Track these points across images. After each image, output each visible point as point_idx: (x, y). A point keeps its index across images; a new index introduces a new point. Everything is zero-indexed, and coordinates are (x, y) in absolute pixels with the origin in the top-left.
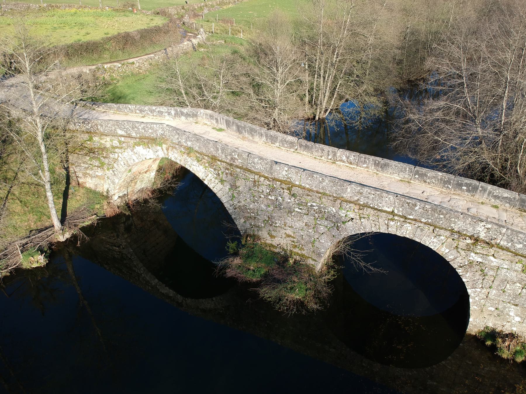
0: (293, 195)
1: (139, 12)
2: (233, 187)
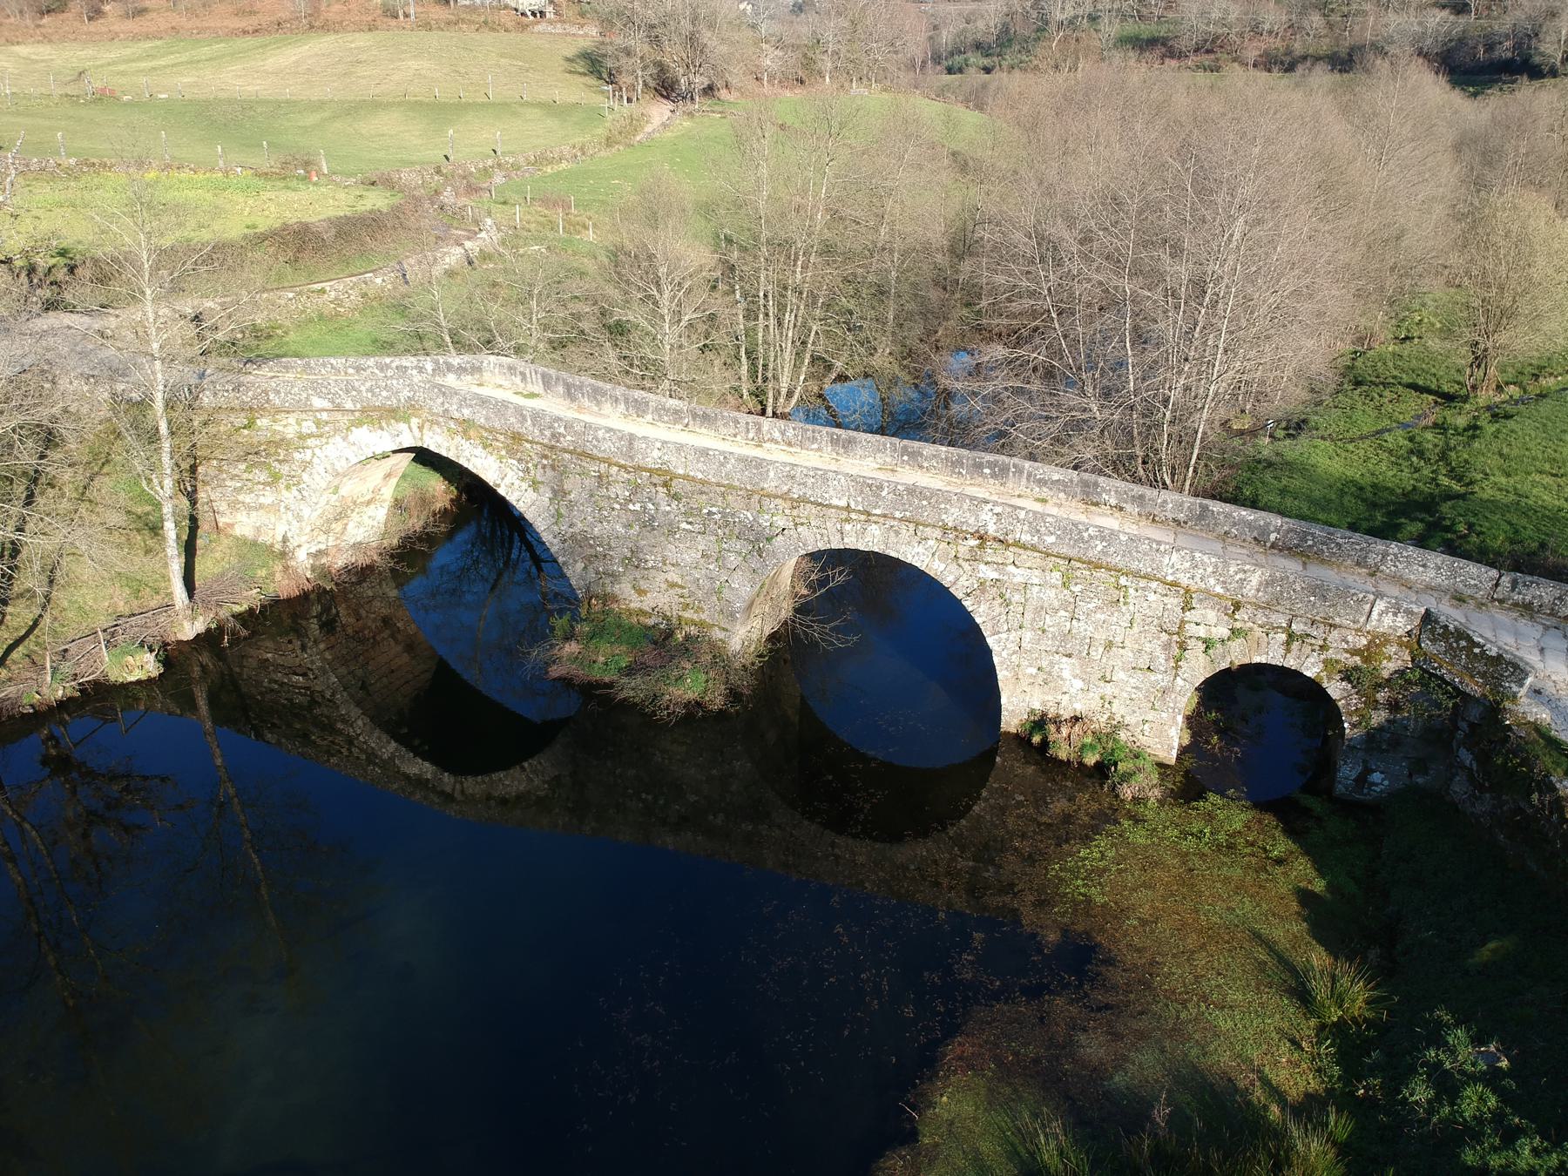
0: (676, 497)
1: (324, 180)
2: (559, 493)
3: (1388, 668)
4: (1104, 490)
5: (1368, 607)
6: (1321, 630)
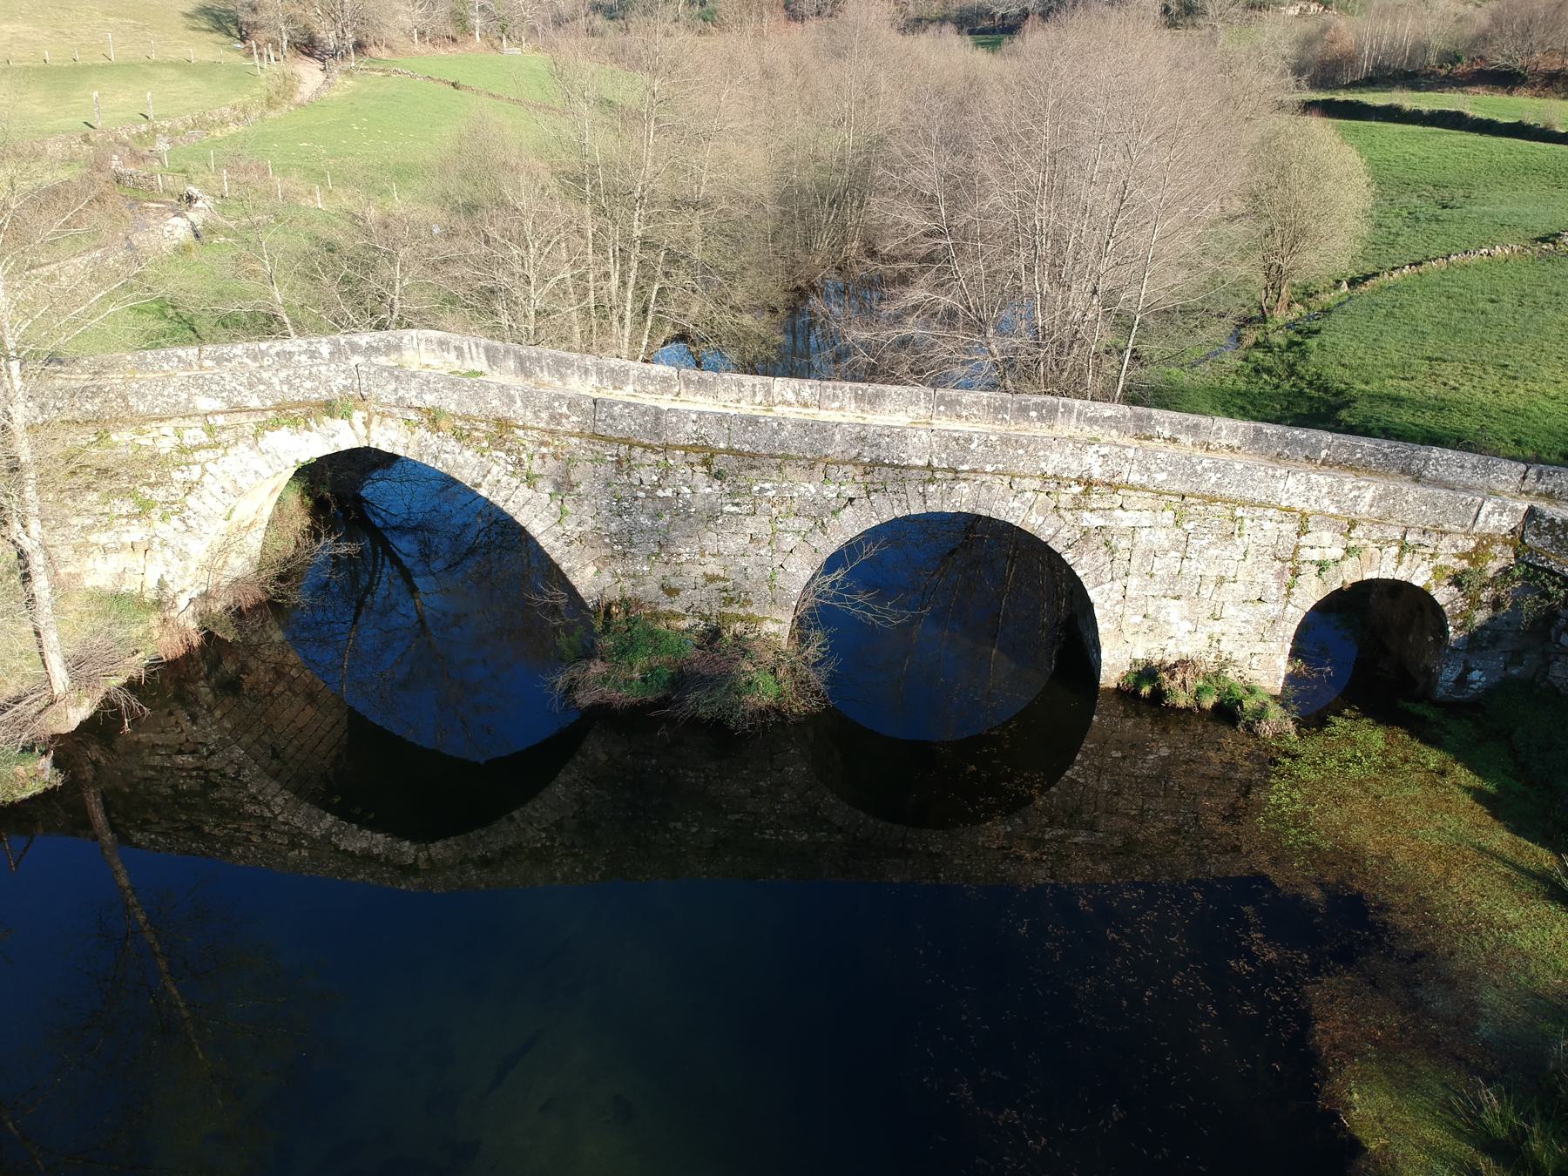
0: (719, 476)
3: (1493, 567)
4: (1158, 423)
5: (1475, 510)
6: (1433, 539)
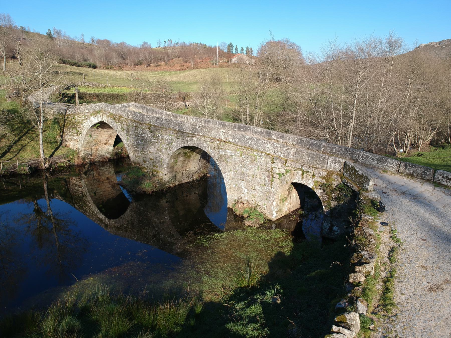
3: (334, 184)
4: (272, 135)
